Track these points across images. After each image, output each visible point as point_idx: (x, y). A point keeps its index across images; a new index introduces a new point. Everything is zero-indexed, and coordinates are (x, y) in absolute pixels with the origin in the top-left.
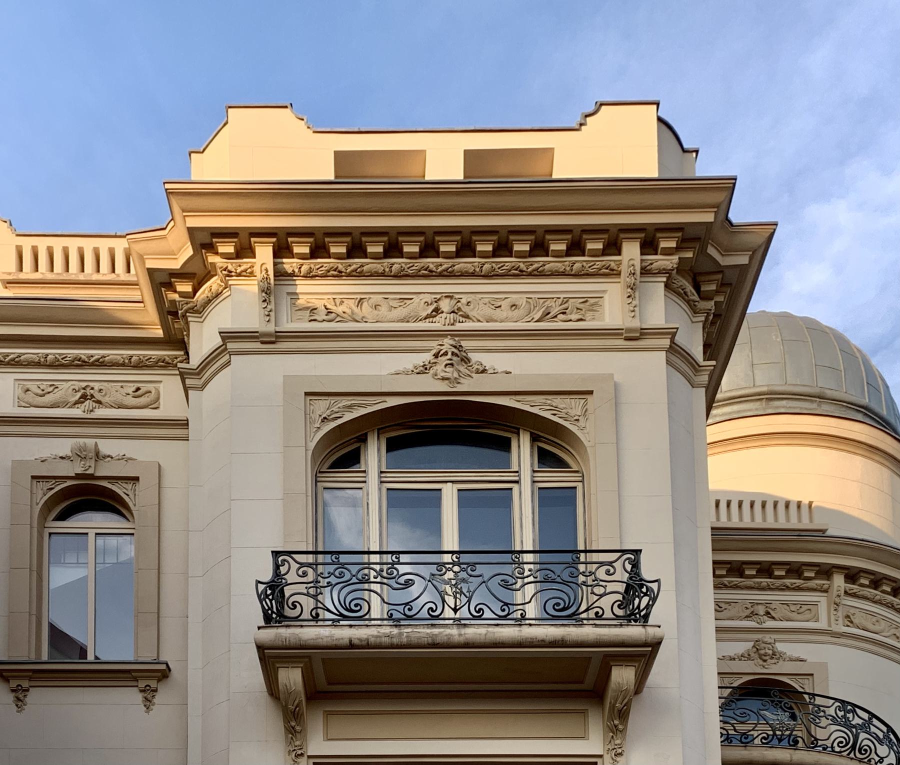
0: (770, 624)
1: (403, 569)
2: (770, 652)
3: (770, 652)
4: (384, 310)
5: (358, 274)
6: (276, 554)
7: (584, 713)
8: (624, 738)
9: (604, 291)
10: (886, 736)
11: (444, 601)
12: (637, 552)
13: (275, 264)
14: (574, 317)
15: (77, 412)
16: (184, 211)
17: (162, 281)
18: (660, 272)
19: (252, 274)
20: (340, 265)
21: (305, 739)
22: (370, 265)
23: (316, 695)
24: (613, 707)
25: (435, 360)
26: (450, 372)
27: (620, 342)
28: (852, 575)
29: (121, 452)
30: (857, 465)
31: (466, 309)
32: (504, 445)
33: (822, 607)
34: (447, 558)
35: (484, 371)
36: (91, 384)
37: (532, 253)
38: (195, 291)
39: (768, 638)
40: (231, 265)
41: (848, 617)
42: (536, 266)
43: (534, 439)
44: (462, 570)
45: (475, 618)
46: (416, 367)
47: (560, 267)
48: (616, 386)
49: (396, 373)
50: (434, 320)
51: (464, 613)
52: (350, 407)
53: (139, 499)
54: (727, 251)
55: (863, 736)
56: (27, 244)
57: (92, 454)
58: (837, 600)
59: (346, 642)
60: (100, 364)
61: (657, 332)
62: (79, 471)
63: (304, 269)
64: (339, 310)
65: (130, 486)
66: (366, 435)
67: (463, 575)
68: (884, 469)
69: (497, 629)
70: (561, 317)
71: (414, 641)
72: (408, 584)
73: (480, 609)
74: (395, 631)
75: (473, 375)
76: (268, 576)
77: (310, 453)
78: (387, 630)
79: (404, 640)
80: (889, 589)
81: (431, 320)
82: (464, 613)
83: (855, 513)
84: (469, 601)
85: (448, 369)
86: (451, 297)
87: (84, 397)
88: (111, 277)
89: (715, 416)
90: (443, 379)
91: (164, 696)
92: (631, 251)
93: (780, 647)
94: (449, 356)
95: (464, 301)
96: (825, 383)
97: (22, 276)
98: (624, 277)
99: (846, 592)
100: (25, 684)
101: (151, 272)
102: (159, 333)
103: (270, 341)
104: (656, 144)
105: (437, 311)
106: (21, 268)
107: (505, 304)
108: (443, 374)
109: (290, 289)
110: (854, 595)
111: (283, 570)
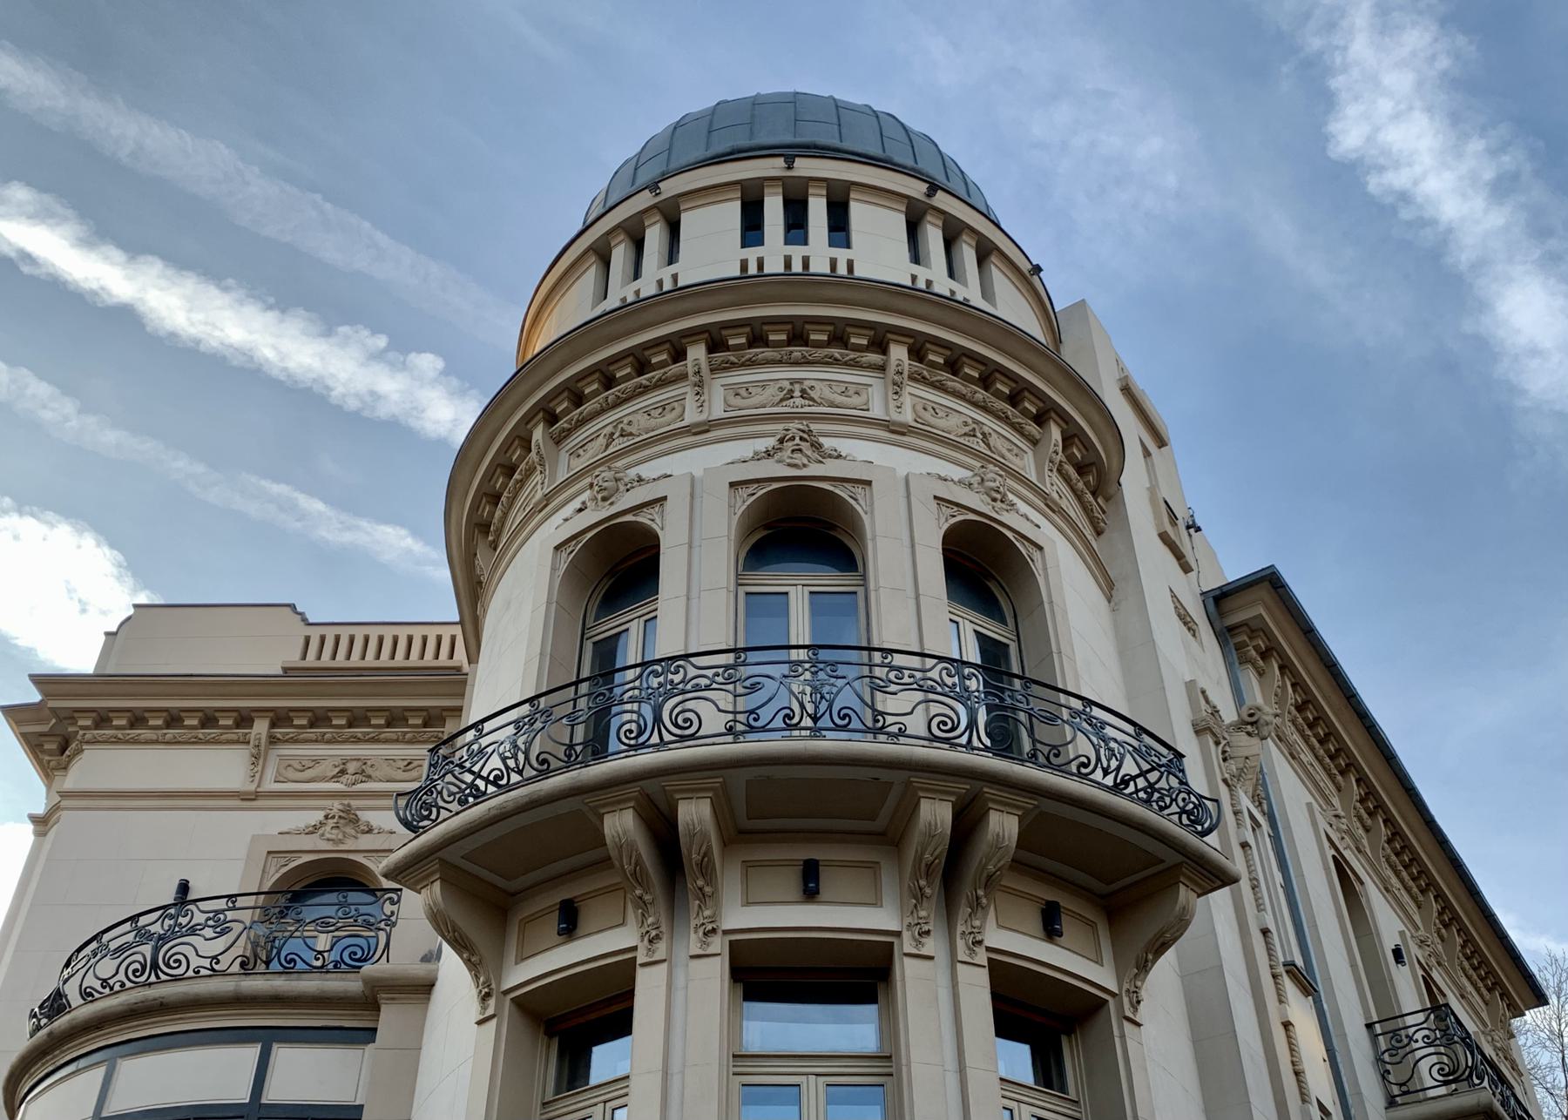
21: (717, 906)
24: (919, 858)
26: (335, 834)
31: (369, 771)
35: (370, 831)
46: (756, 453)
72: (754, 688)
73: (846, 715)
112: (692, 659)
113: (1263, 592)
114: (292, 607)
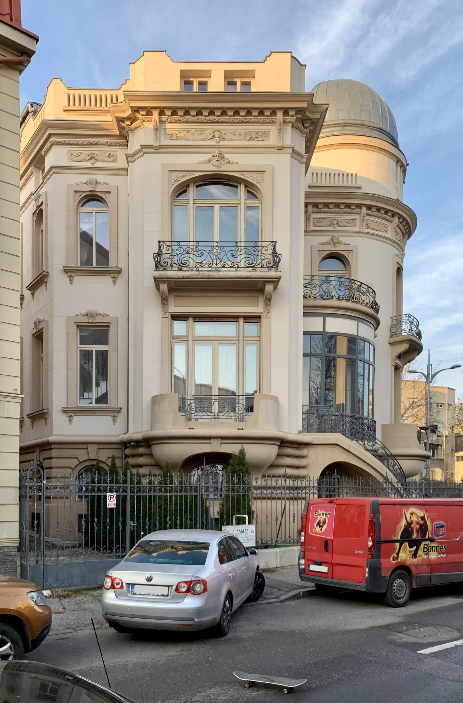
0: (338, 228)
2: (337, 241)
3: (337, 241)
4: (196, 135)
5: (187, 122)
6: (159, 241)
8: (270, 307)
9: (271, 129)
10: (367, 290)
13: (159, 118)
14: (260, 139)
15: (88, 164)
16: (129, 100)
17: (120, 120)
18: (290, 123)
19: (151, 121)
20: (181, 118)
21: (168, 307)
22: (191, 118)
23: (171, 290)
24: (266, 298)
26: (217, 164)
27: (276, 151)
28: (369, 207)
29: (106, 181)
30: (374, 157)
31: (223, 136)
32: (236, 187)
33: (357, 221)
34: (215, 244)
35: (229, 163)
36: (94, 152)
37: (246, 115)
38: (132, 123)
39: (336, 235)
40: (144, 118)
41: (367, 224)
42: (248, 120)
43: (246, 186)
45: (223, 267)
47: (256, 120)
48: (273, 168)
49: (199, 163)
51: (219, 265)
53: (110, 199)
54: (313, 113)
55: (357, 293)
56: (71, 93)
57: (95, 183)
58: (363, 218)
59: (182, 277)
60: (97, 144)
61: (288, 147)
62: (91, 189)
63: (169, 120)
64: (181, 135)
65: (107, 195)
66: (189, 185)
67: (219, 251)
69: (229, 273)
70: (256, 139)
71: (203, 277)
72: (202, 255)
74: (197, 273)
75: (226, 164)
76: (156, 250)
77: (170, 194)
78: (194, 273)
79: (200, 277)
80: (383, 212)
82: (219, 265)
83: (373, 178)
85: (217, 162)
86: (219, 131)
87: (91, 157)
88: (101, 109)
89: (324, 132)
91: (121, 280)
92: (280, 115)
93: (341, 239)
94: (217, 157)
95: (223, 133)
96: (366, 119)
97: (70, 108)
99: (367, 214)
100: (73, 274)
101: (117, 118)
102: (118, 133)
103: (158, 149)
104: (290, 69)
106: (69, 105)
107: (237, 133)
109: (164, 127)
110: (370, 215)
111: (162, 248)
113: (458, 438)
114: (143, 55)
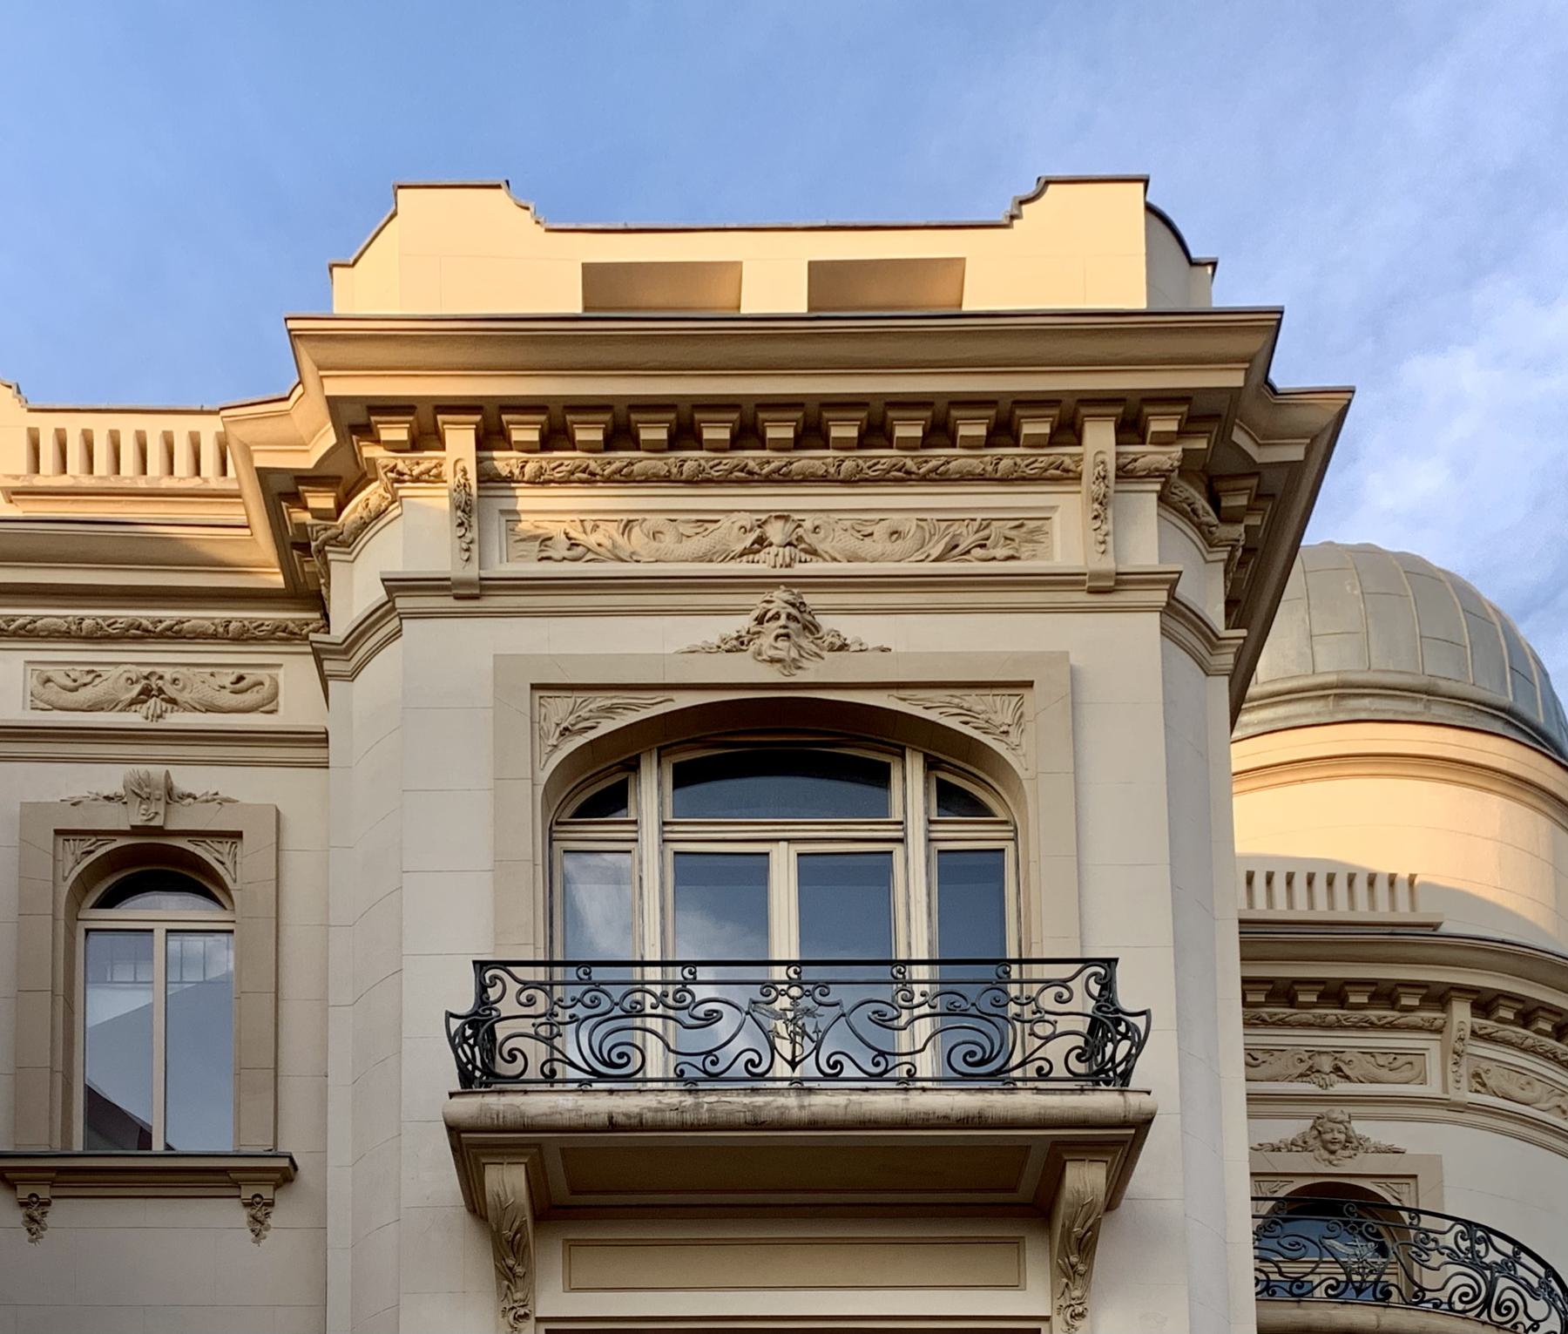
0: (1342, 1088)
1: (701, 992)
2: (1342, 1137)
3: (1342, 1137)
4: (668, 540)
5: (624, 478)
6: (481, 966)
7: (1017, 1243)
8: (1087, 1288)
9: (1053, 508)
10: (1544, 1284)
11: (773, 1048)
12: (1110, 963)
13: (479, 461)
14: (1001, 552)
15: (134, 719)
16: (320, 368)
17: (282, 491)
18: (1150, 474)
19: (439, 478)
20: (593, 461)
21: (531, 1289)
22: (644, 462)
23: (550, 1211)
24: (1067, 1232)
25: (758, 629)
26: (784, 649)
27: (1081, 597)
28: (1484, 1004)
29: (211, 789)
30: (1493, 811)
31: (811, 539)
32: (879, 777)
33: (1432, 1059)
34: (779, 973)
35: (843, 647)
36: (159, 670)
37: (926, 442)
38: (340, 507)
39: (1338, 1112)
40: (402, 462)
41: (1477, 1075)
42: (933, 463)
43: (931, 765)
44: (805, 994)
45: (827, 1077)
46: (724, 640)
47: (975, 465)
48: (1074, 673)
49: (690, 651)
50: (757, 557)
51: (808, 1068)
52: (611, 710)
53: (242, 869)
54: (1266, 437)
55: (1503, 1283)
56: (47, 426)
57: (161, 792)
58: (1459, 1046)
59: (603, 1119)
60: (174, 635)
61: (1145, 580)
62: (138, 821)
63: (530, 469)
64: (591, 540)
65: (226, 848)
66: (637, 759)
67: (807, 1002)
68: (1541, 819)
69: (866, 1097)
70: (978, 552)
71: (722, 1117)
72: (712, 1018)
73: (837, 1062)
74: (689, 1100)
75: (825, 654)
76: (466, 1004)
77: (540, 790)
78: (674, 1099)
79: (705, 1116)
80: (1548, 1028)
81: (751, 557)
82: (808, 1068)
83: (1490, 895)
84: (817, 1049)
85: (781, 644)
86: (786, 518)
87: (147, 693)
88: (194, 483)
89: (1246, 725)
90: (772, 661)
91: (286, 1213)
92: (1100, 437)
93: (1358, 1128)
94: (783, 621)
95: (808, 525)
96: (1438, 669)
97: (39, 482)
98: (1088, 484)
99: (1473, 1033)
100: (44, 1192)
101: (263, 474)
102: (277, 580)
103: (471, 594)
104: (1143, 250)
105: (761, 542)
106: (36, 468)
107: (880, 531)
108: (772, 653)
109: (506, 504)
110: (1488, 1038)
111: (493, 993)
112: (512, 969)
